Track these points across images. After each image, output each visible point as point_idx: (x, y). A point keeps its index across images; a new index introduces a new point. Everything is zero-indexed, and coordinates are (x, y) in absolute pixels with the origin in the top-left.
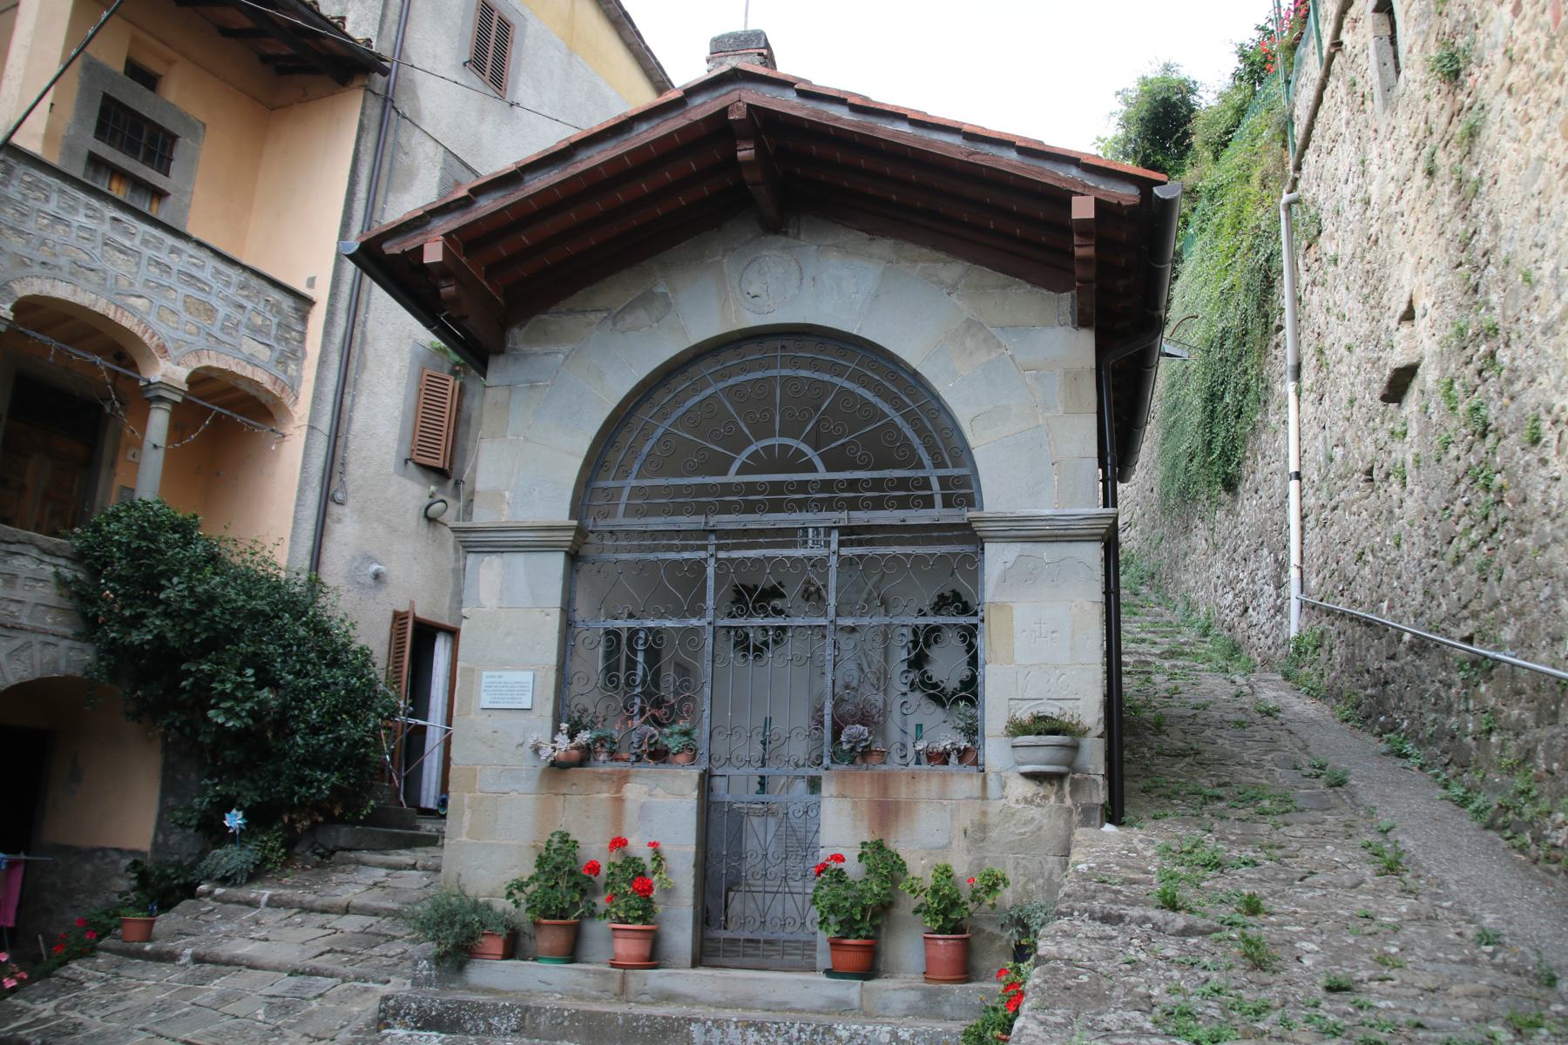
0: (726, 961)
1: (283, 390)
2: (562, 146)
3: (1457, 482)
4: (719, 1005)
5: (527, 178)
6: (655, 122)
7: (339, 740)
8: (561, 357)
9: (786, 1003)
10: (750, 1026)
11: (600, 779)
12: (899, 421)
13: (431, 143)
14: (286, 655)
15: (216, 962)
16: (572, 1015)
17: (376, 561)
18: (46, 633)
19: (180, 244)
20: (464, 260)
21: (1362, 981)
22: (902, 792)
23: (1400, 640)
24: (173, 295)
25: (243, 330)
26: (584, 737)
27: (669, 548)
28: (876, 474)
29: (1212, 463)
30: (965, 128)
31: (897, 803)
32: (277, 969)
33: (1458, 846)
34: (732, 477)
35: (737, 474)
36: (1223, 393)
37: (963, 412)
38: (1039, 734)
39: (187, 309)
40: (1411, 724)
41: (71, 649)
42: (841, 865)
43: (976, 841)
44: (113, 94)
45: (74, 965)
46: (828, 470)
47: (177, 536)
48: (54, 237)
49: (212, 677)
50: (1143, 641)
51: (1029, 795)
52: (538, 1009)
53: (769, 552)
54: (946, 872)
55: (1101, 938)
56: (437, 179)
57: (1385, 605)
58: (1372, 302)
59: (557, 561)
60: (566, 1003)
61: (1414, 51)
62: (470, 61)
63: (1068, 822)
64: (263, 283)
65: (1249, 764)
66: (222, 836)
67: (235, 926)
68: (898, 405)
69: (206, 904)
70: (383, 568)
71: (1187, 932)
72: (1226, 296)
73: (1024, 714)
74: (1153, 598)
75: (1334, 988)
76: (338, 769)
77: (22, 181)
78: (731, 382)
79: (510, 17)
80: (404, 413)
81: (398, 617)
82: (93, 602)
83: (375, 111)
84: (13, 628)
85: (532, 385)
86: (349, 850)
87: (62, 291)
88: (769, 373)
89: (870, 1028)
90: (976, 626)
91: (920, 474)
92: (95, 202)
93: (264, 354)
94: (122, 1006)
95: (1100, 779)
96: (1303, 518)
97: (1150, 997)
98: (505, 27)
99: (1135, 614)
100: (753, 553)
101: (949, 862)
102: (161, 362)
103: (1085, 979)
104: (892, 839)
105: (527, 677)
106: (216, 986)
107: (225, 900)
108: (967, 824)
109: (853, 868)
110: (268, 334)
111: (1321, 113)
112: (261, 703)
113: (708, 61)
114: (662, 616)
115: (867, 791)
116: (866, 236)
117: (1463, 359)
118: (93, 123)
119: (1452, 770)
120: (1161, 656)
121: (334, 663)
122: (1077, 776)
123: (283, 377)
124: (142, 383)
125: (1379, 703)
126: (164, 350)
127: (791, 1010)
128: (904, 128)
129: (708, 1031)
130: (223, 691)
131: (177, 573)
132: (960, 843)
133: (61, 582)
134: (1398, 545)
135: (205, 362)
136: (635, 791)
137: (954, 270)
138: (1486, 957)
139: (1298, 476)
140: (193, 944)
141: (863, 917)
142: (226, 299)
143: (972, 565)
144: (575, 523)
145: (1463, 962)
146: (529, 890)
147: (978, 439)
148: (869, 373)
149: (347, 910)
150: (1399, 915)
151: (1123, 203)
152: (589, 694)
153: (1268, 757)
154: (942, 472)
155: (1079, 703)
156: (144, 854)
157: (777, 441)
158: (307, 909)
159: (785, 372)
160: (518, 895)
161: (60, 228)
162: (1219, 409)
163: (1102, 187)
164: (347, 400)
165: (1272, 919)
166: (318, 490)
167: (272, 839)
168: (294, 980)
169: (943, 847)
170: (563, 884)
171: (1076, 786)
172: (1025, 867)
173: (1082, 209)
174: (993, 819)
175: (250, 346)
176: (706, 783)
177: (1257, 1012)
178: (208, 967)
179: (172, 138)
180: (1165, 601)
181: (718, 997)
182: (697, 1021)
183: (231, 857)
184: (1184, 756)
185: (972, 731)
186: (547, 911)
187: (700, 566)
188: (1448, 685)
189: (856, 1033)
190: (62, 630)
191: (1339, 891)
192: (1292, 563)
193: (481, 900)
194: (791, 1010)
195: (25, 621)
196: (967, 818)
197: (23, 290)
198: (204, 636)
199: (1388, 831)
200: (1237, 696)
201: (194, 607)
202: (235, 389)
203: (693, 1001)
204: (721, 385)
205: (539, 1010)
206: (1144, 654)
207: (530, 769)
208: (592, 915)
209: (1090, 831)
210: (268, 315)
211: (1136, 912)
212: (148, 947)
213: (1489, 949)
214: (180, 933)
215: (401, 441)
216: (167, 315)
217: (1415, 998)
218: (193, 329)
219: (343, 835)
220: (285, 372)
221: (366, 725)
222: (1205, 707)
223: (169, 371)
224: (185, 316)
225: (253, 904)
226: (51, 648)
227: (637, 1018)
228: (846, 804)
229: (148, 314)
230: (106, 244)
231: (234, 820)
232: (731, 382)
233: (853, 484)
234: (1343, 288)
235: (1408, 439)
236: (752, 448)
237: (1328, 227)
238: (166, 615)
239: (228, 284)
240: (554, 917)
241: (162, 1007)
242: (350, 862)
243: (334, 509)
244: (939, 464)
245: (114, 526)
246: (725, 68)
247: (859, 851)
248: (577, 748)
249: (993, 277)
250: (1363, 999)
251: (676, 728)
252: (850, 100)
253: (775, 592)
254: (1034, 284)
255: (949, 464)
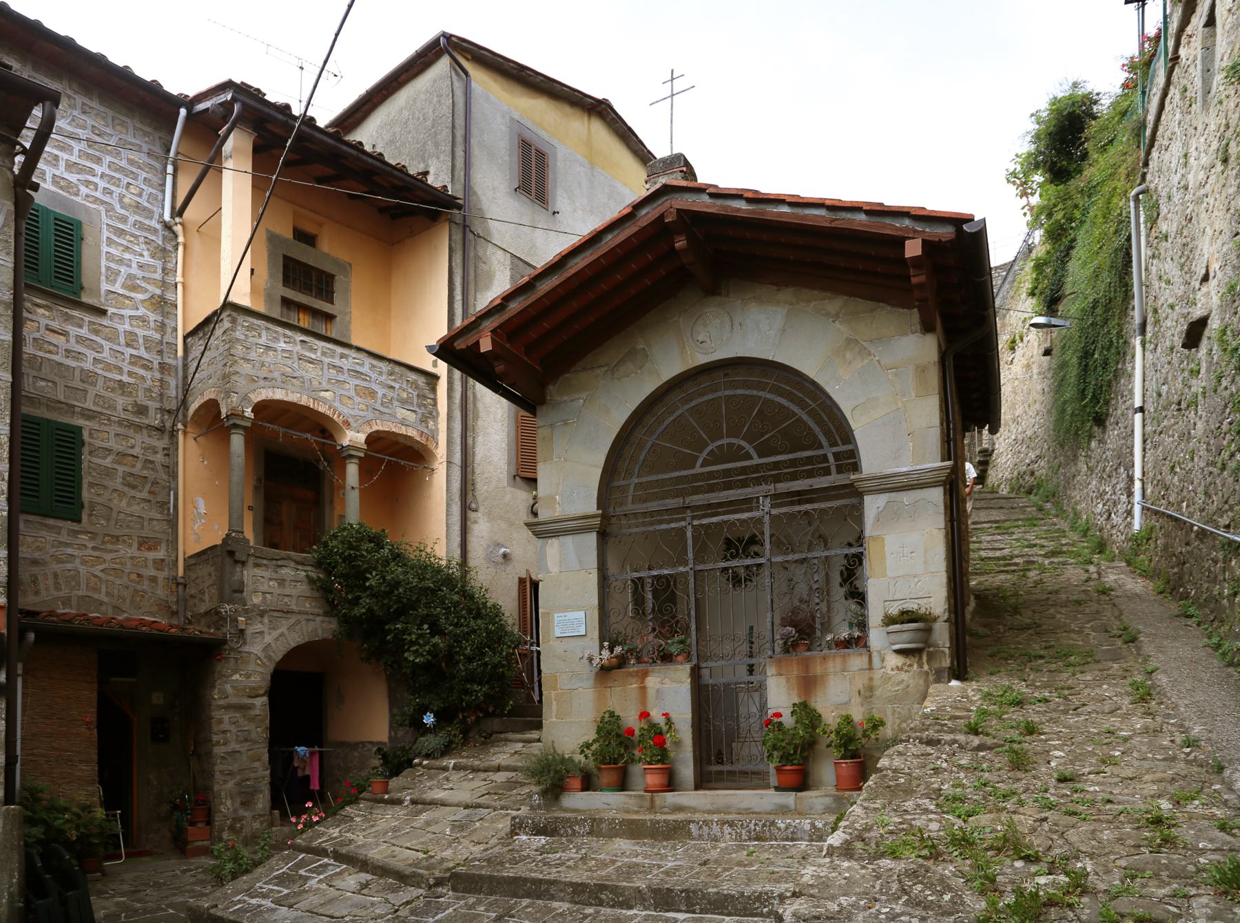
0: (717, 785)
1: (427, 439)
2: (557, 259)
3: (1226, 406)
4: (710, 812)
5: (538, 284)
6: (616, 232)
7: (486, 664)
8: (581, 401)
9: (749, 809)
10: (725, 823)
11: (632, 676)
12: (805, 417)
13: (500, 252)
14: (448, 613)
15: (424, 803)
16: (620, 822)
17: (503, 546)
18: (307, 613)
19: (346, 351)
20: (508, 345)
21: (1083, 775)
22: (818, 669)
23: (1192, 530)
24: (347, 386)
25: (396, 403)
26: (618, 650)
27: (661, 522)
28: (791, 456)
29: (1085, 406)
30: (827, 203)
31: (815, 676)
32: (457, 805)
33: (1201, 680)
34: (698, 470)
35: (701, 466)
36: (1094, 350)
37: (846, 407)
38: (903, 623)
39: (358, 394)
40: (1196, 592)
41: (323, 622)
42: (779, 720)
43: (866, 697)
44: (289, 255)
45: (348, 808)
46: (760, 457)
47: (372, 545)
48: (269, 360)
49: (404, 631)
50: (1035, 545)
51: (900, 665)
52: (601, 819)
53: (725, 518)
54: (848, 720)
55: (922, 755)
56: (508, 277)
57: (1185, 504)
58: (1186, 269)
59: (591, 539)
60: (618, 816)
61: (1225, 58)
62: (519, 187)
63: (926, 681)
64: (403, 369)
65: (1074, 631)
66: (423, 730)
67: (435, 782)
68: (802, 404)
69: (419, 771)
70: (508, 551)
71: (981, 747)
72: (1096, 275)
73: (894, 610)
74: (1053, 512)
75: (1063, 780)
76: (488, 682)
77: (243, 326)
78: (693, 404)
79: (543, 148)
80: (509, 445)
81: (522, 581)
82: (331, 592)
83: (458, 237)
84: (288, 612)
85: (565, 423)
86: (501, 733)
87: (279, 395)
88: (716, 395)
89: (798, 821)
90: (862, 553)
91: (821, 452)
92: (288, 332)
93: (411, 417)
94: (373, 830)
95: (947, 651)
96: (1144, 441)
97: (941, 790)
98: (541, 155)
99: (1035, 525)
100: (715, 520)
101: (849, 713)
102: (347, 432)
103: (902, 780)
104: (813, 699)
105: (581, 615)
106: (424, 817)
107: (428, 767)
108: (861, 687)
109: (788, 720)
110: (412, 404)
111: (1163, 117)
112: (435, 645)
113: (646, 182)
114: (661, 567)
115: (795, 671)
116: (775, 288)
117: (1233, 311)
118: (281, 276)
119: (1216, 624)
120: (1046, 556)
121: (478, 616)
122: (931, 649)
123: (426, 431)
124: (338, 448)
125: (1181, 578)
126: (347, 424)
127: (753, 813)
128: (785, 209)
129: (701, 827)
130: (411, 640)
131: (375, 569)
132: (856, 700)
133: (311, 581)
134: (1192, 459)
135: (375, 428)
136: (652, 682)
137: (835, 304)
138: (1183, 756)
139: (1142, 410)
140: (411, 794)
141: (795, 752)
142: (381, 383)
143: (857, 513)
144: (600, 512)
145: (1164, 760)
146: (594, 747)
147: (858, 425)
148: (783, 386)
149: (498, 769)
150: (1134, 730)
151: (943, 240)
152: (623, 619)
153: (1088, 625)
154: (835, 449)
155: (931, 600)
156: (385, 744)
157: (725, 441)
158: (475, 770)
159: (727, 393)
160: (587, 752)
161: (271, 353)
162: (1091, 363)
163: (927, 230)
164: (470, 441)
165: (1043, 737)
166: (459, 503)
167: (454, 730)
168: (467, 811)
169: (846, 703)
170: (613, 744)
171: (931, 657)
172: (899, 713)
173: (913, 249)
174: (876, 682)
175: (402, 413)
176: (696, 674)
177: (1004, 796)
178: (420, 806)
179: (331, 277)
180: (1061, 513)
181: (709, 807)
182: (693, 822)
183: (430, 742)
184: (1029, 629)
185: (863, 625)
186: (605, 759)
187: (682, 531)
188: (1215, 561)
189: (790, 825)
190: (316, 611)
191: (1100, 716)
192: (1136, 478)
193: (567, 756)
194: (753, 813)
195: (294, 607)
196: (860, 683)
197: (257, 398)
198: (395, 607)
199: (1152, 672)
200: (1087, 581)
201: (387, 589)
202: (397, 443)
203: (694, 810)
204: (687, 407)
205: (601, 820)
206: (1032, 555)
207: (587, 673)
208: (633, 760)
209: (940, 686)
210: (410, 390)
211: (948, 737)
212: (386, 797)
213: (1188, 750)
214: (405, 788)
215: (509, 464)
216: (346, 400)
217: (1116, 784)
218: (364, 407)
219: (495, 723)
220: (427, 427)
221: (501, 654)
222: (1057, 592)
223: (354, 437)
224: (358, 400)
225: (445, 769)
226: (312, 623)
227: (658, 822)
228: (783, 680)
229: (334, 401)
230: (300, 359)
231: (429, 719)
232: (693, 404)
233: (776, 465)
234: (1169, 259)
235: (1200, 376)
236: (710, 448)
237: (1164, 210)
238: (372, 596)
239: (381, 373)
240: (610, 764)
241: (395, 830)
242: (502, 740)
243: (471, 515)
244: (833, 444)
245: (335, 543)
246: (658, 186)
247: (792, 709)
248: (616, 657)
249: (863, 304)
250: (1079, 786)
251: (676, 639)
252: (746, 195)
253: (753, 540)
254: (893, 305)
255: (840, 443)
